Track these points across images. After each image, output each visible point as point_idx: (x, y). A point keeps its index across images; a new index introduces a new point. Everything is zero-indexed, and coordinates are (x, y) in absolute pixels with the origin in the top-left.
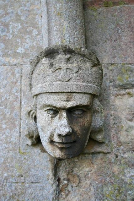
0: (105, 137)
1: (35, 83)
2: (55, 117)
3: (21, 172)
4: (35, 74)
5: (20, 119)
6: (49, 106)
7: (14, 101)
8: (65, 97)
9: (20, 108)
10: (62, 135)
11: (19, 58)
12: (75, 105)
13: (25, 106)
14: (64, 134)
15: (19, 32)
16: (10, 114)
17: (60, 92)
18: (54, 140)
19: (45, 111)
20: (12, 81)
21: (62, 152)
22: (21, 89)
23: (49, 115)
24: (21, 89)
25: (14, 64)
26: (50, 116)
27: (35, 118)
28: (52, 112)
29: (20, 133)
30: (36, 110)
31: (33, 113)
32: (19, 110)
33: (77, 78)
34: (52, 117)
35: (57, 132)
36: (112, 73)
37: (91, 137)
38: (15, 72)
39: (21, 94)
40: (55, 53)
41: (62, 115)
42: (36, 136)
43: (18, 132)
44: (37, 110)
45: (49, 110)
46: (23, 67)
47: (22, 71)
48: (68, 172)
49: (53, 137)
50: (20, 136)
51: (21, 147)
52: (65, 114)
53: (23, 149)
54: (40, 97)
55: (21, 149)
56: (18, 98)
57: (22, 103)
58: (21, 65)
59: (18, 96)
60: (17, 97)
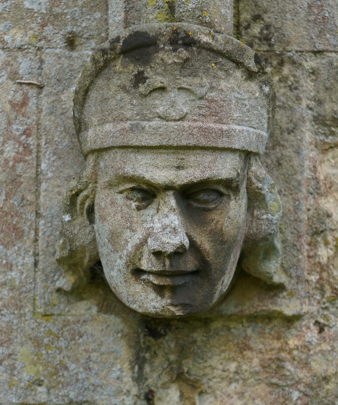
0: (24, 103)
1: (95, 120)
2: (145, 207)
3: (38, 372)
4: (93, 94)
5: (38, 215)
6: (132, 179)
7: (17, 161)
8: (172, 159)
9: (37, 180)
10: (165, 252)
11: (33, 25)
12: (108, 279)
13: (50, 175)
14: (170, 249)
15: (290, 399)
16: (6, 200)
17: (160, 147)
18: (142, 268)
19: (121, 192)
20: (10, 97)
21: (162, 296)
22: (38, 124)
23: (132, 202)
24: (38, 124)
25: (18, 43)
26: (134, 205)
27: (91, 211)
28: (139, 196)
29: (36, 255)
30: (94, 191)
31: (87, 197)
32: (33, 189)
33: (203, 111)
34: (139, 209)
35: (153, 245)
36: (316, 80)
37: (246, 270)
38: (21, 72)
39: (39, 139)
40: (148, 46)
41: (264, 194)
42: (89, 261)
43: (31, 253)
44: (99, 189)
45: (133, 189)
46: (43, 57)
47: (40, 68)
48: (176, 372)
49: (140, 259)
50: (36, 264)
51: (37, 298)
52: (173, 202)
53: (45, 303)
54: (107, 156)
55: (38, 303)
56: (31, 152)
57: (43, 166)
58: (39, 49)
59: (29, 145)
60: (27, 148)
